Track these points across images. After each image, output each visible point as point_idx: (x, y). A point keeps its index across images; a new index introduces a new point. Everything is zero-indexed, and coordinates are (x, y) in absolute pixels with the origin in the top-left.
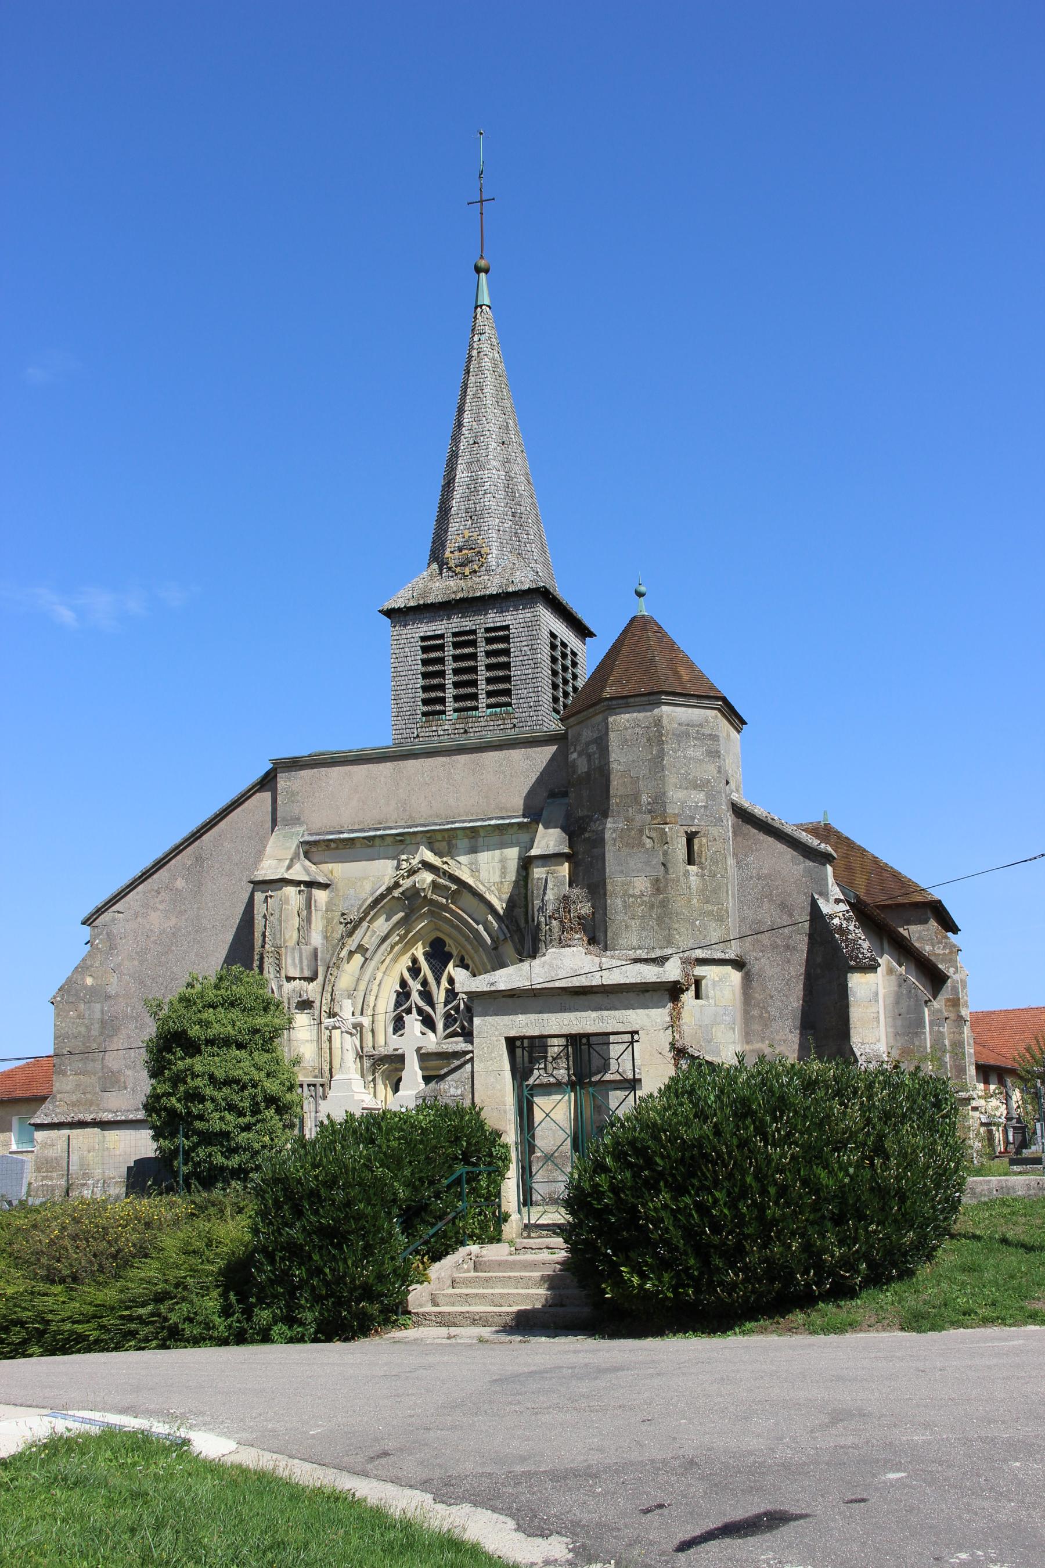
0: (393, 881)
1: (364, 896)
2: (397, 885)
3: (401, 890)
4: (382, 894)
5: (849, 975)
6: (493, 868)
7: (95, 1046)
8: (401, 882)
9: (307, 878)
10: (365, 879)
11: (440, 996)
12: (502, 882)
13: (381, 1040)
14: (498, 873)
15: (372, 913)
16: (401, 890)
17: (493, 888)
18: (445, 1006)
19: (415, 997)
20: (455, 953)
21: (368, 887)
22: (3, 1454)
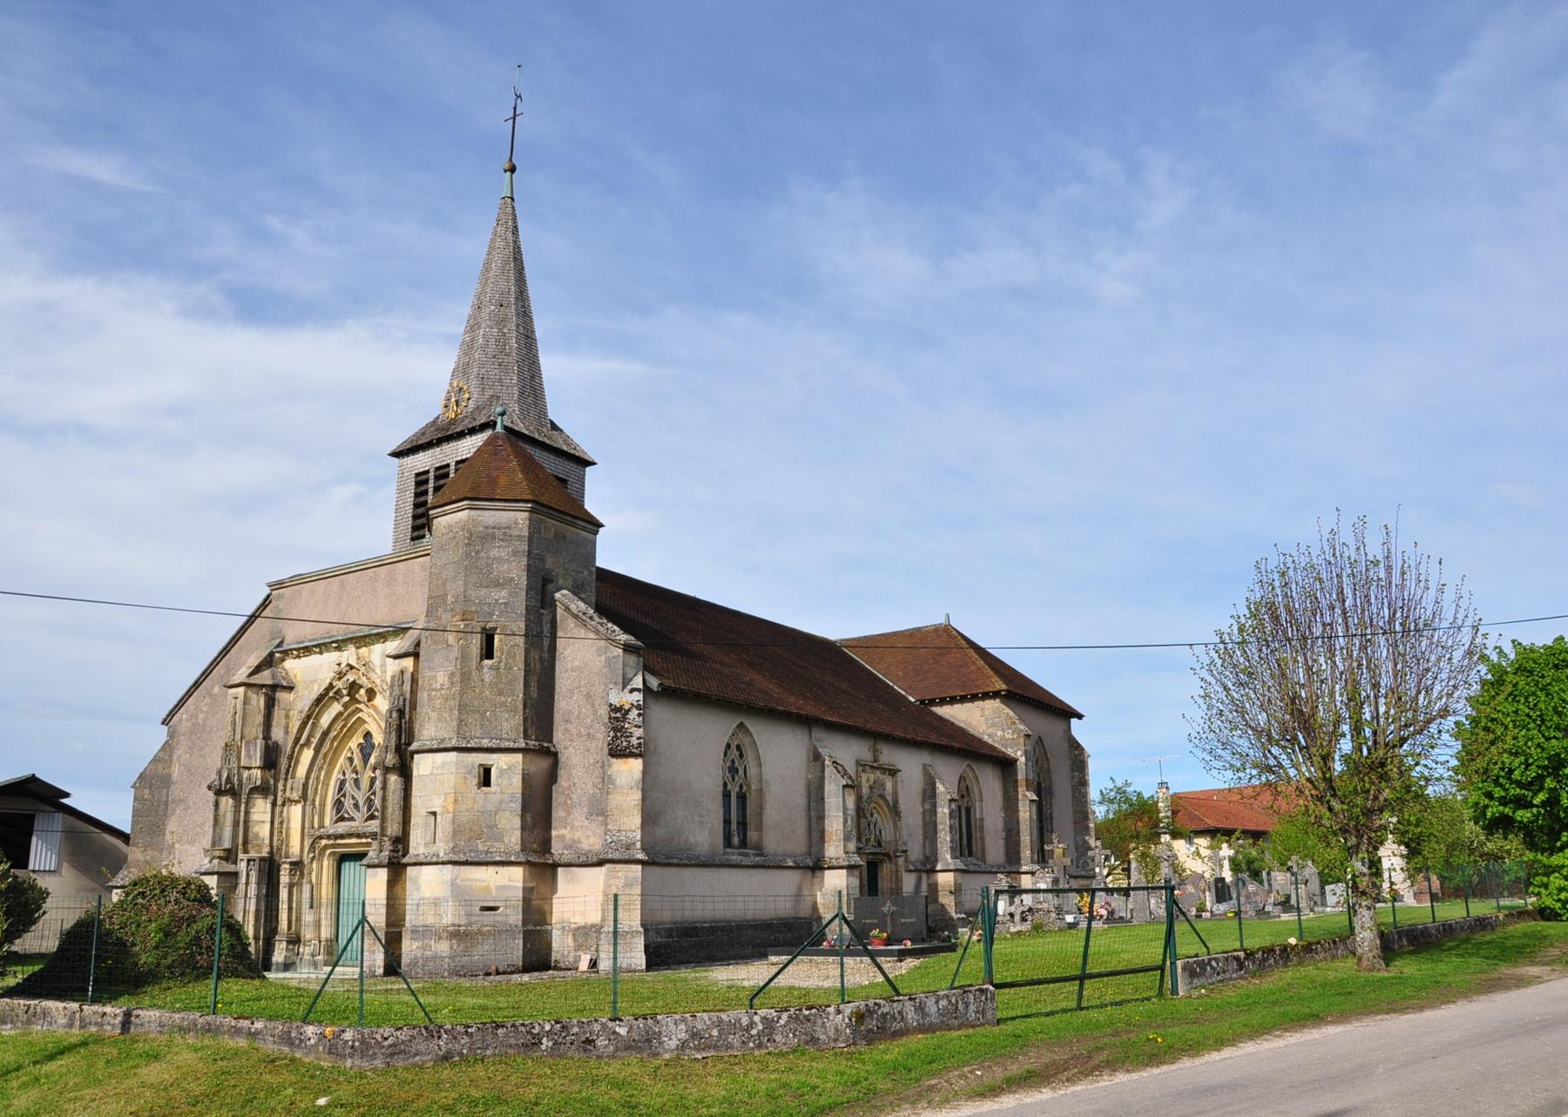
11: (365, 784)
13: (327, 822)
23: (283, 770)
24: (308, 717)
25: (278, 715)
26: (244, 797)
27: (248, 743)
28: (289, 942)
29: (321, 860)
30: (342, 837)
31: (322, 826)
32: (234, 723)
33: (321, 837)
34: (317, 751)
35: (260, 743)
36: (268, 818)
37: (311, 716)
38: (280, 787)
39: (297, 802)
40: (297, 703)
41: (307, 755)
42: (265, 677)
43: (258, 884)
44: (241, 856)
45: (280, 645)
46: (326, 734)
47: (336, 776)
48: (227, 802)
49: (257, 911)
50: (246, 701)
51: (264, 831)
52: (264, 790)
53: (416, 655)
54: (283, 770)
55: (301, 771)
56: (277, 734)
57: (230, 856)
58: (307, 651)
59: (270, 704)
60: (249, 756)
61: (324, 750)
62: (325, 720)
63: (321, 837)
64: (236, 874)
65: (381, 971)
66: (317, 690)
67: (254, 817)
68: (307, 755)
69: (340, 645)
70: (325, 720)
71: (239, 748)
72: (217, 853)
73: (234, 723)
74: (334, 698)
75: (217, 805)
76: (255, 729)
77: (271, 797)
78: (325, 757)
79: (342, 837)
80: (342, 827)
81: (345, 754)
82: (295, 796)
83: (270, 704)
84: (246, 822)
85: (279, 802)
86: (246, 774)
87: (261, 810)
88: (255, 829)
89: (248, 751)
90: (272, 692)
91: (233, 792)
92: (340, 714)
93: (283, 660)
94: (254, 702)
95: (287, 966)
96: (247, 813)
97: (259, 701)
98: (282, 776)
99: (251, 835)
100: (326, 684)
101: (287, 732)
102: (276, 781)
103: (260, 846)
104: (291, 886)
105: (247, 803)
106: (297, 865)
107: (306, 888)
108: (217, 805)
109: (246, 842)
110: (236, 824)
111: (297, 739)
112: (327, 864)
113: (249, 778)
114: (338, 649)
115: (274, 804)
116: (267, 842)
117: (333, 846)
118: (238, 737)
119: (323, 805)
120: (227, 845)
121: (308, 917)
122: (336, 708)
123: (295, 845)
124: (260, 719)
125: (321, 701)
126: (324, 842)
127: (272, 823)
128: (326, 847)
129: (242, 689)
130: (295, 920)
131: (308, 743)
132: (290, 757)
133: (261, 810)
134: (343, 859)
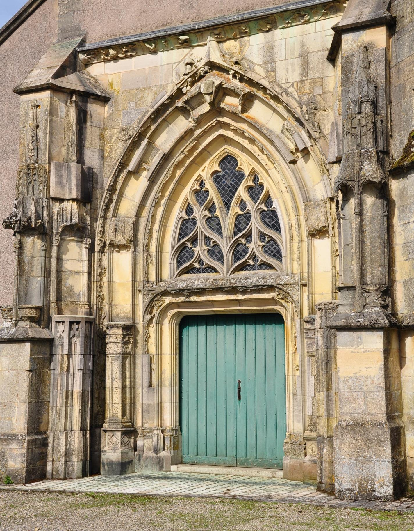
0: (176, 88)
1: (144, 108)
2: (179, 93)
3: (185, 98)
4: (163, 104)
5: (342, 36)
6: (292, 65)
7: (115, 161)
8: (184, 90)
9: (81, 88)
10: (145, 89)
11: (228, 223)
12: (302, 81)
13: (166, 273)
14: (298, 70)
15: (153, 127)
16: (185, 98)
17: (291, 90)
18: (235, 233)
19: (201, 227)
20: (247, 172)
21: (149, 98)
22: (395, 3)
23: (101, 206)
24: (141, 136)
25: (91, 133)
26: (56, 237)
27: (59, 167)
28: (125, 433)
29: (160, 323)
30: (202, 292)
31: (159, 280)
32: (36, 139)
33: (165, 293)
34: (152, 180)
35: (74, 168)
36: (84, 267)
37: (142, 136)
38: (98, 228)
39: (125, 247)
40: (112, 124)
41: (136, 188)
42: (71, 81)
43: (84, 355)
44: (55, 317)
45: (82, 43)
46: (166, 158)
47: (177, 212)
48: (34, 244)
49: (83, 391)
50: (53, 111)
51: (79, 284)
52: (78, 231)
53: (391, 25)
54: (101, 206)
55: (128, 206)
56: (92, 158)
57: (42, 318)
58: (131, 48)
59: (82, 117)
60: (60, 184)
61: (162, 179)
62: (165, 141)
63: (165, 293)
64: (50, 342)
65: (389, 490)
66: (150, 103)
67: (68, 266)
68: (136, 188)
69: (190, 37)
70: (165, 141)
71: (48, 172)
72: (28, 313)
73: (36, 139)
74: (184, 111)
75: (21, 247)
76: (65, 149)
77: (87, 241)
78: (165, 186)
79: (202, 292)
80: (197, 280)
81: (192, 184)
82: (121, 239)
83: (82, 117)
84: (59, 271)
85: (97, 248)
86: (56, 208)
87: (75, 255)
88: (69, 282)
89: (59, 177)
90: (86, 98)
91: (42, 232)
92: (189, 132)
93: (87, 64)
94: (62, 113)
95: (124, 467)
96: (59, 259)
97: (69, 113)
98: (101, 213)
99: (64, 289)
100: (170, 90)
101: (102, 157)
102: (94, 219)
103: (75, 304)
104: (124, 357)
105: (59, 247)
106: (129, 329)
107: (141, 361)
108: (21, 247)
109: (59, 299)
110: (47, 274)
111: (123, 165)
112: (168, 327)
113: (61, 214)
114: (186, 44)
115: (91, 249)
116: (84, 299)
117: (178, 305)
118: (44, 157)
119: (160, 252)
120: (36, 301)
121: (144, 398)
122: (181, 124)
123: (123, 302)
124: (71, 136)
125: (161, 114)
126: (168, 300)
127: (89, 274)
128: (171, 306)
129: (46, 94)
130: (128, 404)
131: (136, 172)
132: (112, 189)
133: (75, 255)
134: (185, 322)
